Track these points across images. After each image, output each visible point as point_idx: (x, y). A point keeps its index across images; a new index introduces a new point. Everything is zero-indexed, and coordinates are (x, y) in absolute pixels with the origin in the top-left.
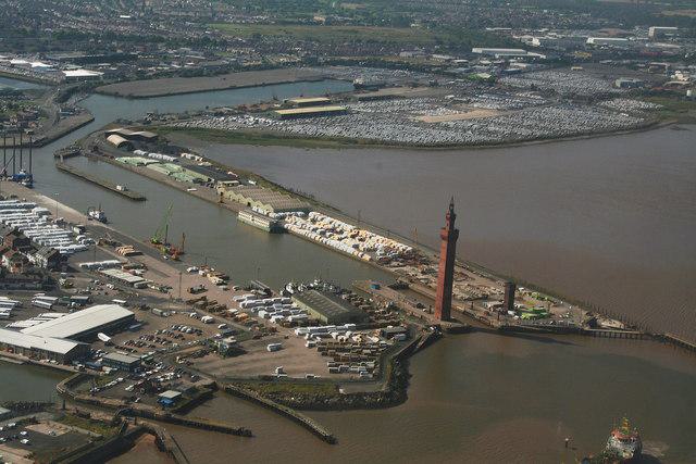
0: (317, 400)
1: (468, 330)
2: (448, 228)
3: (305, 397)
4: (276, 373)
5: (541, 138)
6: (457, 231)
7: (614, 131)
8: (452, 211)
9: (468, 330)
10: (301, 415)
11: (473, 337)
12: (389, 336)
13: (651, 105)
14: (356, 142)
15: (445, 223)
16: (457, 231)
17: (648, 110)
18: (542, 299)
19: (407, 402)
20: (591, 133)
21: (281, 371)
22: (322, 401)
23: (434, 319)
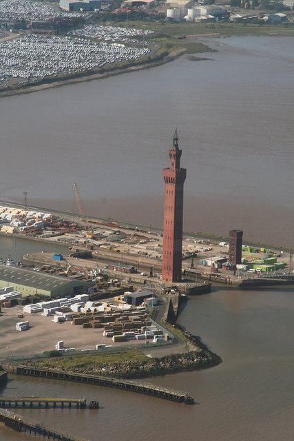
0: (132, 368)
1: (206, 290)
2: (173, 168)
3: (117, 366)
4: (57, 347)
5: (47, 80)
6: (184, 171)
7: (125, 67)
8: (176, 146)
9: (206, 290)
10: (131, 382)
11: (213, 295)
12: (139, 301)
13: (138, 32)
14: (115, 68)
15: (169, 163)
16: (184, 171)
17: (137, 37)
18: (257, 251)
19: (220, 365)
20: (102, 71)
21: (62, 345)
22: (137, 368)
23: (163, 281)
